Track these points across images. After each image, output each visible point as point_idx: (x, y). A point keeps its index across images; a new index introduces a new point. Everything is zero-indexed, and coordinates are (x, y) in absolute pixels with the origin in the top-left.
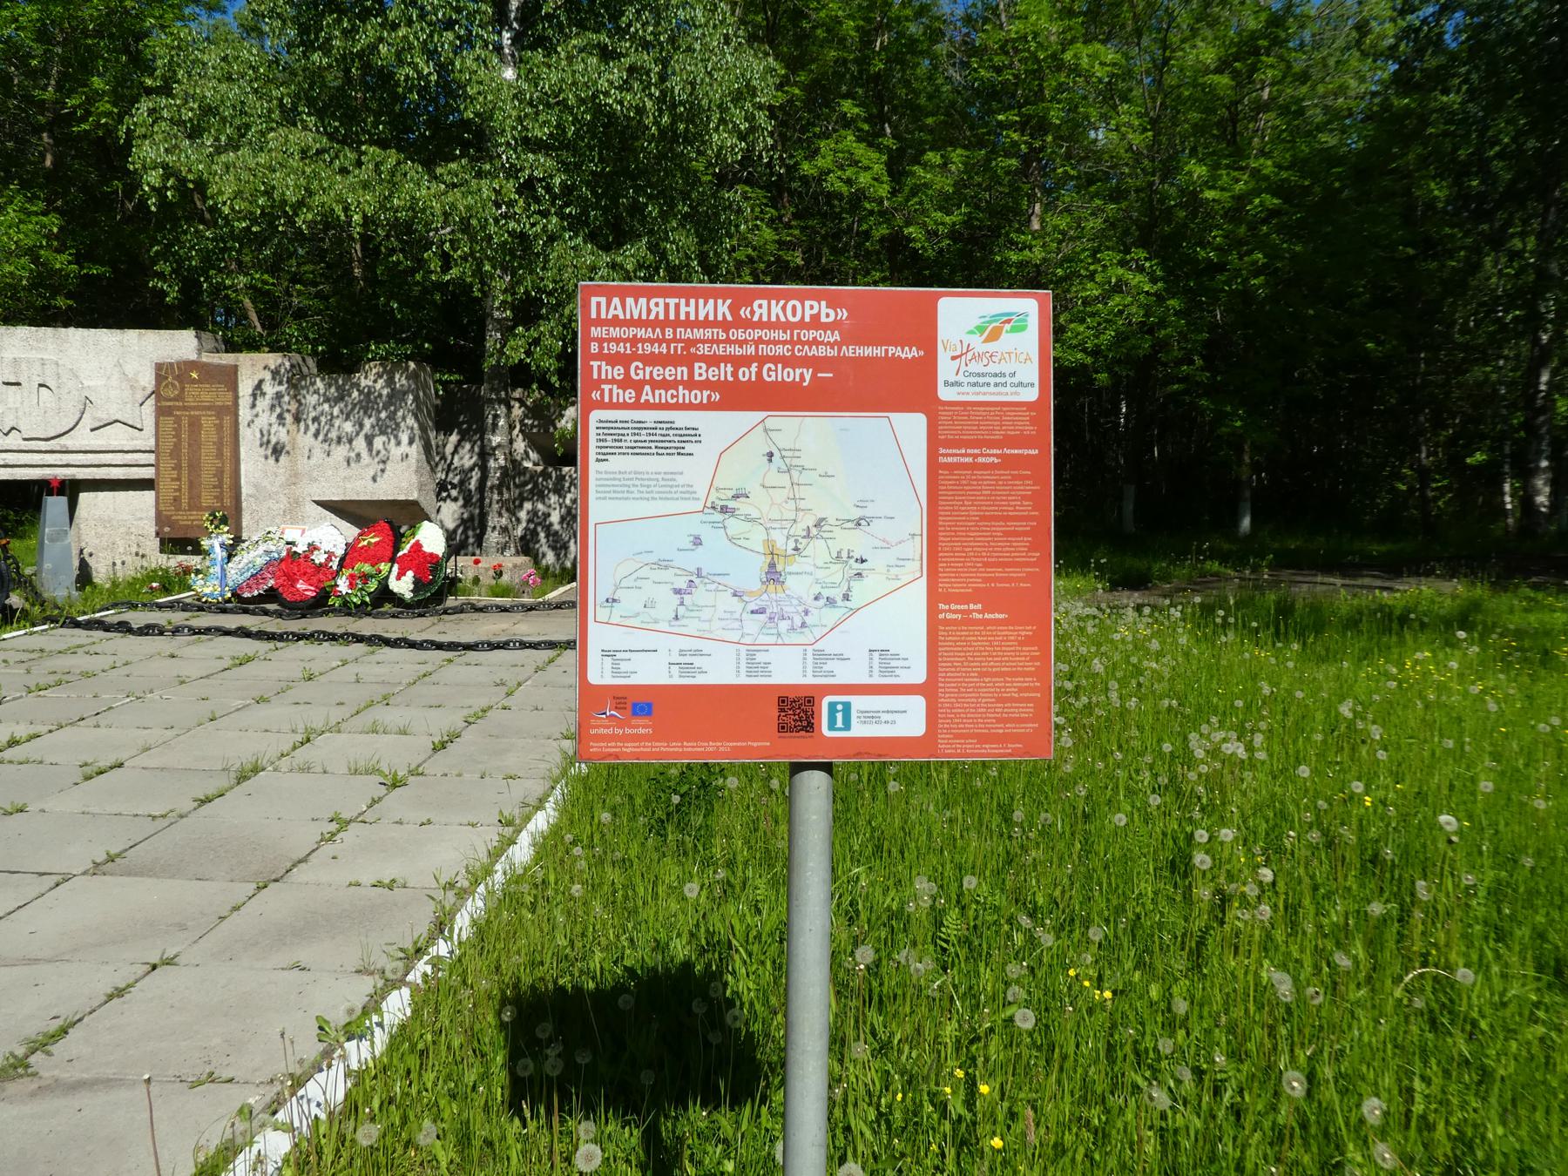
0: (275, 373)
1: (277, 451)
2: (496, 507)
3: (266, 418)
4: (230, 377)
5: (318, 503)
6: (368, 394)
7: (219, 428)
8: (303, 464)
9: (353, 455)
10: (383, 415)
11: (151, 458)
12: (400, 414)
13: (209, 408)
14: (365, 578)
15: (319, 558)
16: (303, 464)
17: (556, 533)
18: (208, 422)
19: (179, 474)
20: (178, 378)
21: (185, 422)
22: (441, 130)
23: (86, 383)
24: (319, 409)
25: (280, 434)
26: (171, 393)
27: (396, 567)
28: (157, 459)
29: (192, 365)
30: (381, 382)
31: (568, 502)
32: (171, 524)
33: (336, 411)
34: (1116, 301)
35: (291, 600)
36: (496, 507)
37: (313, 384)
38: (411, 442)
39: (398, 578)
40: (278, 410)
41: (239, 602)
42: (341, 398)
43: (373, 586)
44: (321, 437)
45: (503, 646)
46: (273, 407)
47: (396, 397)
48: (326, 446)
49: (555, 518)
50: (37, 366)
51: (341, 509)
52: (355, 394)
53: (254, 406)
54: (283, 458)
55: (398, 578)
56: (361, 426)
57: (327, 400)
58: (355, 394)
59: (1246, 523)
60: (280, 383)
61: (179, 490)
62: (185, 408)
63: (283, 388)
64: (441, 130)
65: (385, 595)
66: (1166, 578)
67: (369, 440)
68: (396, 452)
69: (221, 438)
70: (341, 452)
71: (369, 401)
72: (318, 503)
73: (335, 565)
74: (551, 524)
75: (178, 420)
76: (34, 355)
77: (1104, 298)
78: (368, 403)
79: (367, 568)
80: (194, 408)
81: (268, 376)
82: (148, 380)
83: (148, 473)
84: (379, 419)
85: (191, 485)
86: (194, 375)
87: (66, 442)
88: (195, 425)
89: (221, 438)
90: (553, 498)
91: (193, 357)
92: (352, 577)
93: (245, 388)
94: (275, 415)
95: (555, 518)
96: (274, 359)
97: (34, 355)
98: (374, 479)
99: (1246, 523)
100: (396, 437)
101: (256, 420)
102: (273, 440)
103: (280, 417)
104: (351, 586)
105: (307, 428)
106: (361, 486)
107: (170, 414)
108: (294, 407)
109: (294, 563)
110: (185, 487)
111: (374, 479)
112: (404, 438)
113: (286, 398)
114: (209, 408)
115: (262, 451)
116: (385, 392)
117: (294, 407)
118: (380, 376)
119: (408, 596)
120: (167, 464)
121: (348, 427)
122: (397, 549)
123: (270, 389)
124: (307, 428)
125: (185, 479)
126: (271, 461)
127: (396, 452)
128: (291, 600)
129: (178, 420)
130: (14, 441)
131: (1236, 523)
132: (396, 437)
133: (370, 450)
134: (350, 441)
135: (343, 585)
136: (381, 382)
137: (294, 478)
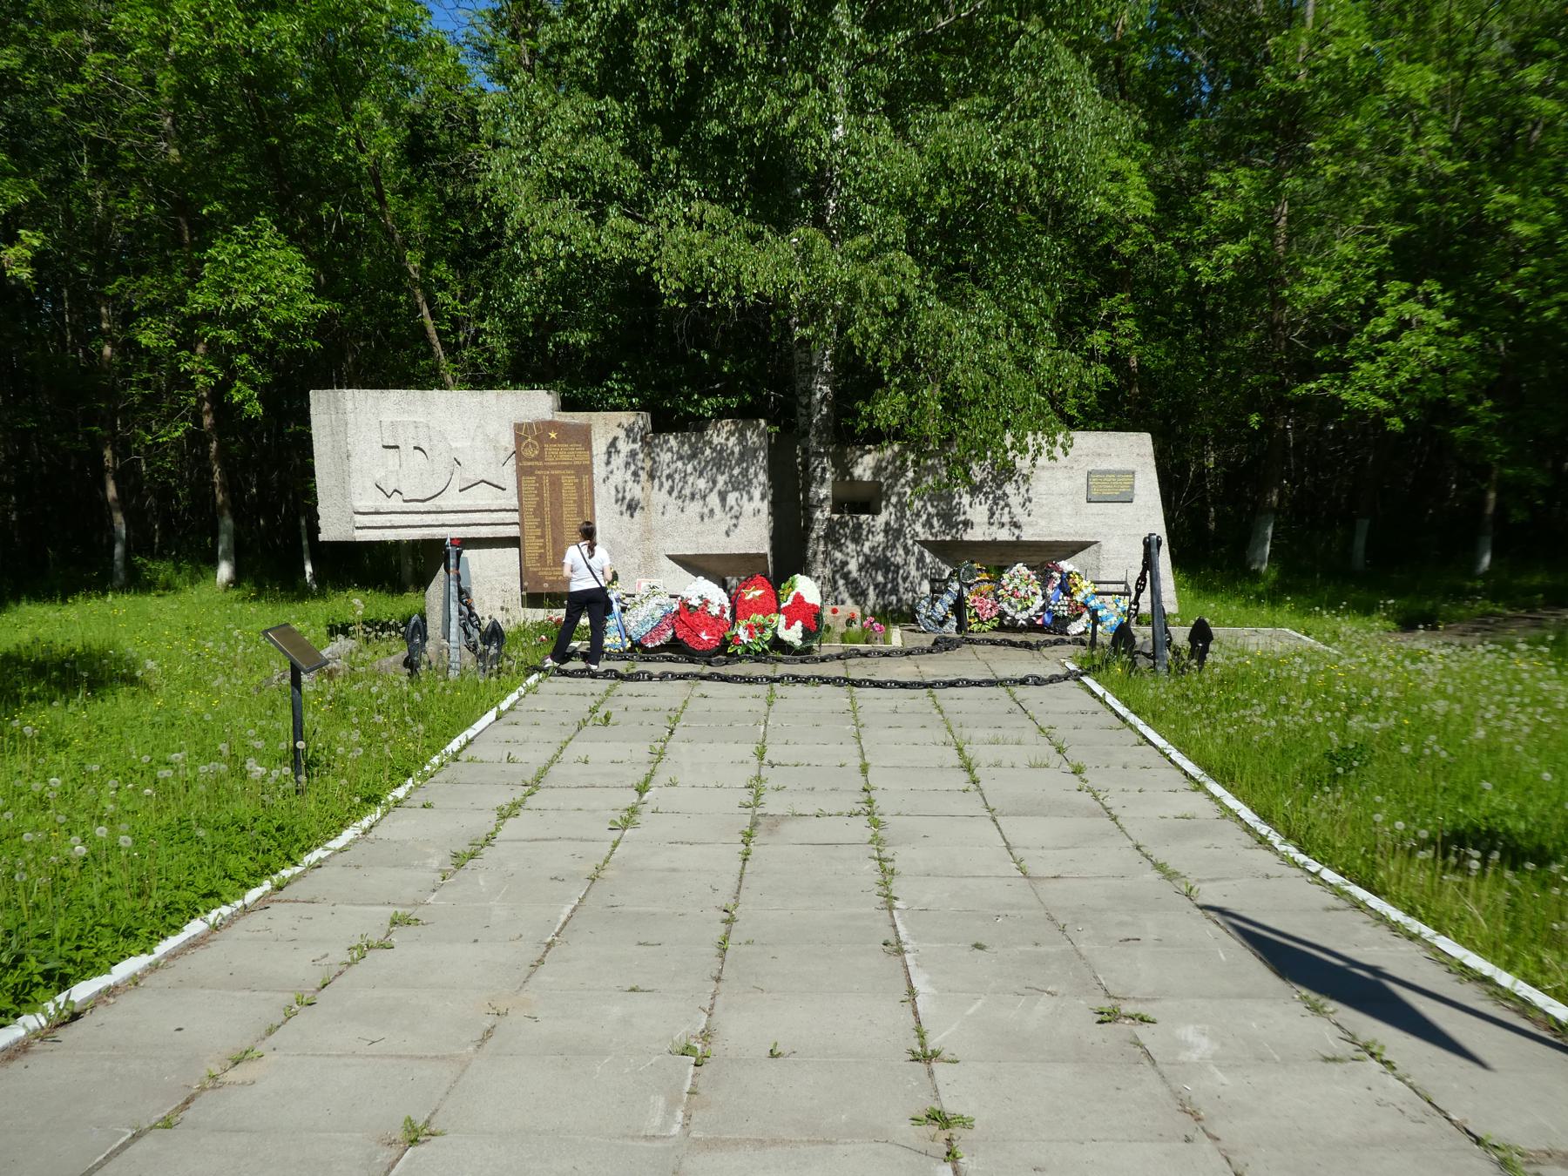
0: (629, 431)
1: (632, 507)
2: (820, 557)
3: (621, 476)
4: (583, 436)
5: (671, 557)
6: (720, 451)
7: (579, 486)
8: (656, 519)
9: (706, 511)
10: (736, 472)
11: (515, 517)
12: (752, 471)
13: (568, 467)
14: (762, 628)
15: (715, 611)
16: (656, 519)
17: (855, 580)
18: (568, 482)
19: (543, 532)
20: (537, 438)
21: (546, 481)
22: (775, 186)
23: (454, 445)
24: (673, 467)
25: (634, 491)
26: (530, 453)
27: (783, 618)
28: (521, 516)
29: (551, 425)
30: (733, 440)
31: (866, 550)
32: (539, 580)
33: (689, 468)
34: (1407, 340)
35: (686, 645)
36: (820, 557)
37: (666, 442)
38: (763, 498)
39: (788, 626)
40: (633, 468)
41: (662, 648)
42: (693, 456)
43: (768, 634)
44: (675, 494)
45: (952, 684)
46: (627, 465)
47: (747, 454)
48: (680, 502)
49: (853, 566)
50: (411, 428)
51: (694, 564)
52: (708, 451)
53: (608, 463)
54: (637, 514)
55: (788, 626)
56: (715, 482)
57: (681, 458)
58: (708, 451)
59: (1486, 560)
60: (634, 441)
61: (544, 547)
62: (545, 468)
63: (637, 446)
64: (775, 186)
65: (778, 644)
66: (1448, 620)
67: (723, 497)
68: (748, 507)
69: (581, 497)
70: (695, 508)
71: (722, 458)
72: (671, 557)
73: (727, 615)
74: (850, 572)
75: (539, 479)
76: (405, 418)
77: (1393, 336)
78: (721, 460)
79: (758, 618)
80: (553, 467)
81: (622, 434)
82: (508, 440)
83: (513, 531)
84: (731, 476)
85: (555, 541)
86: (553, 435)
87: (439, 503)
88: (556, 484)
89: (581, 497)
90: (851, 547)
91: (549, 417)
92: (749, 627)
93: (599, 446)
94: (629, 472)
95: (853, 566)
96: (627, 418)
97: (405, 418)
98: (727, 534)
99: (1486, 560)
100: (748, 492)
101: (610, 476)
102: (628, 497)
103: (635, 474)
104: (751, 635)
105: (661, 485)
106: (714, 541)
107: (532, 474)
108: (648, 464)
109: (687, 614)
110: (549, 545)
111: (727, 534)
112: (757, 494)
113: (641, 456)
114: (568, 467)
115: (617, 508)
116: (737, 450)
117: (648, 464)
118: (731, 433)
119: (798, 643)
120: (531, 522)
121: (702, 484)
122: (779, 604)
123: (624, 447)
124: (661, 485)
125: (549, 536)
126: (626, 517)
127: (748, 507)
128: (686, 645)
129: (539, 479)
130: (396, 503)
131: (1476, 561)
132: (748, 492)
133: (724, 506)
134: (704, 497)
135: (744, 636)
136: (733, 440)
137: (648, 533)
